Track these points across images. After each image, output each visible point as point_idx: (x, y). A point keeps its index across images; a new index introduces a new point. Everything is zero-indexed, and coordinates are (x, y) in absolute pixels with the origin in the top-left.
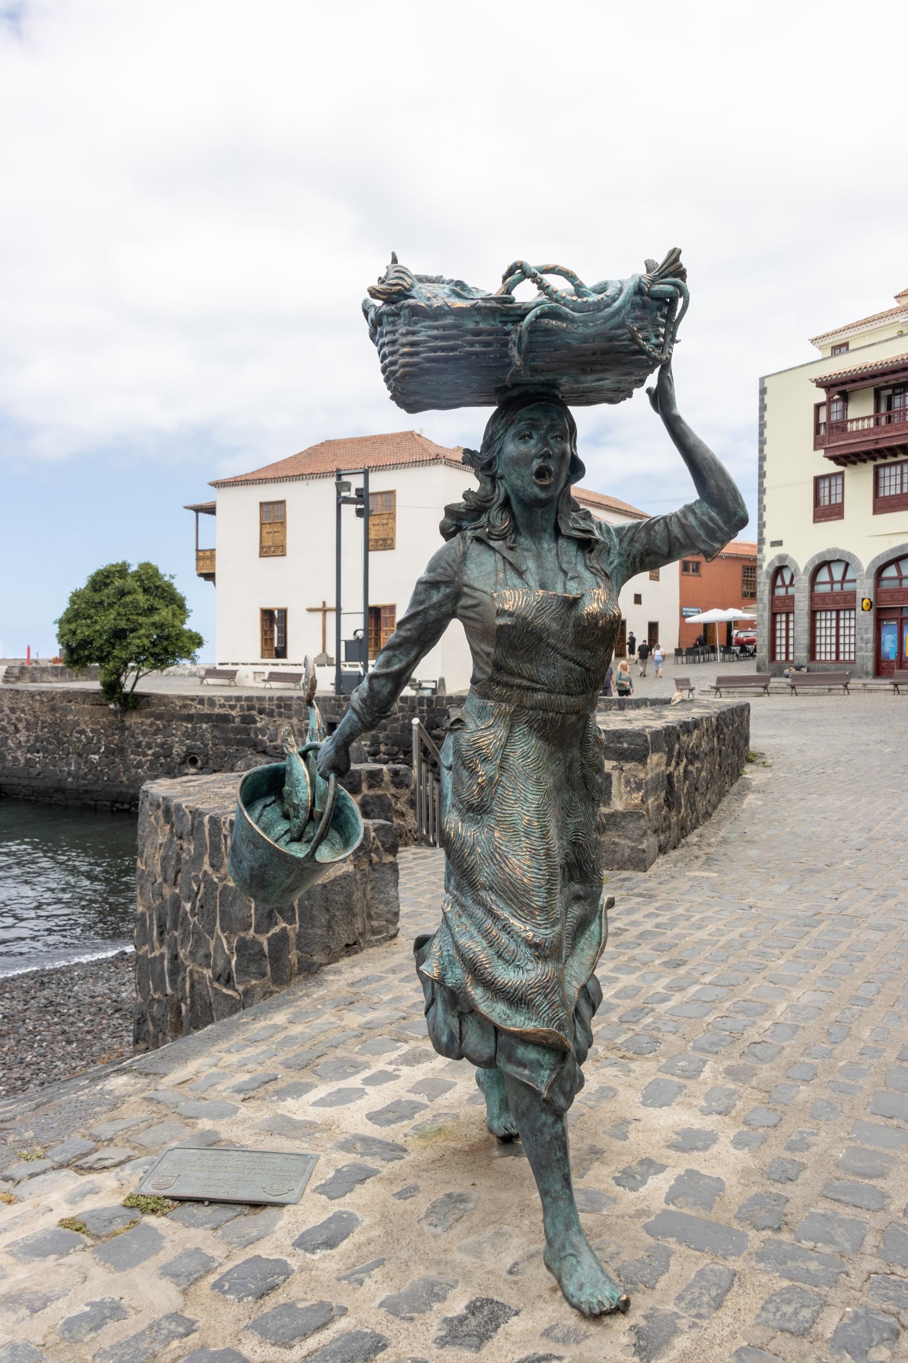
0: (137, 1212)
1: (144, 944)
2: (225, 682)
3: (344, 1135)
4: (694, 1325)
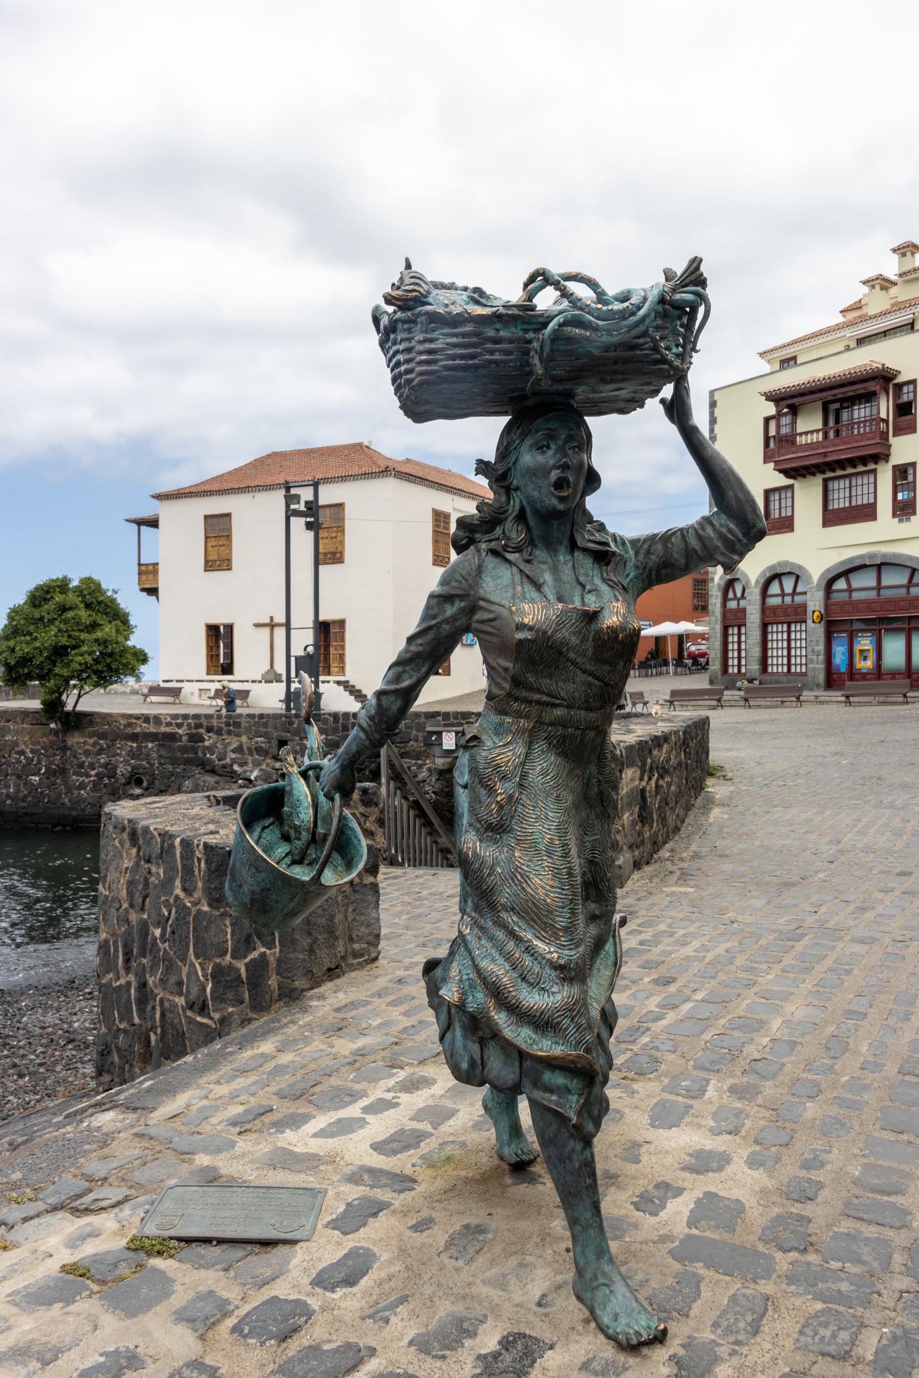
0: (142, 1255)
1: (108, 972)
2: (170, 699)
3: (350, 1167)
4: (733, 1353)
